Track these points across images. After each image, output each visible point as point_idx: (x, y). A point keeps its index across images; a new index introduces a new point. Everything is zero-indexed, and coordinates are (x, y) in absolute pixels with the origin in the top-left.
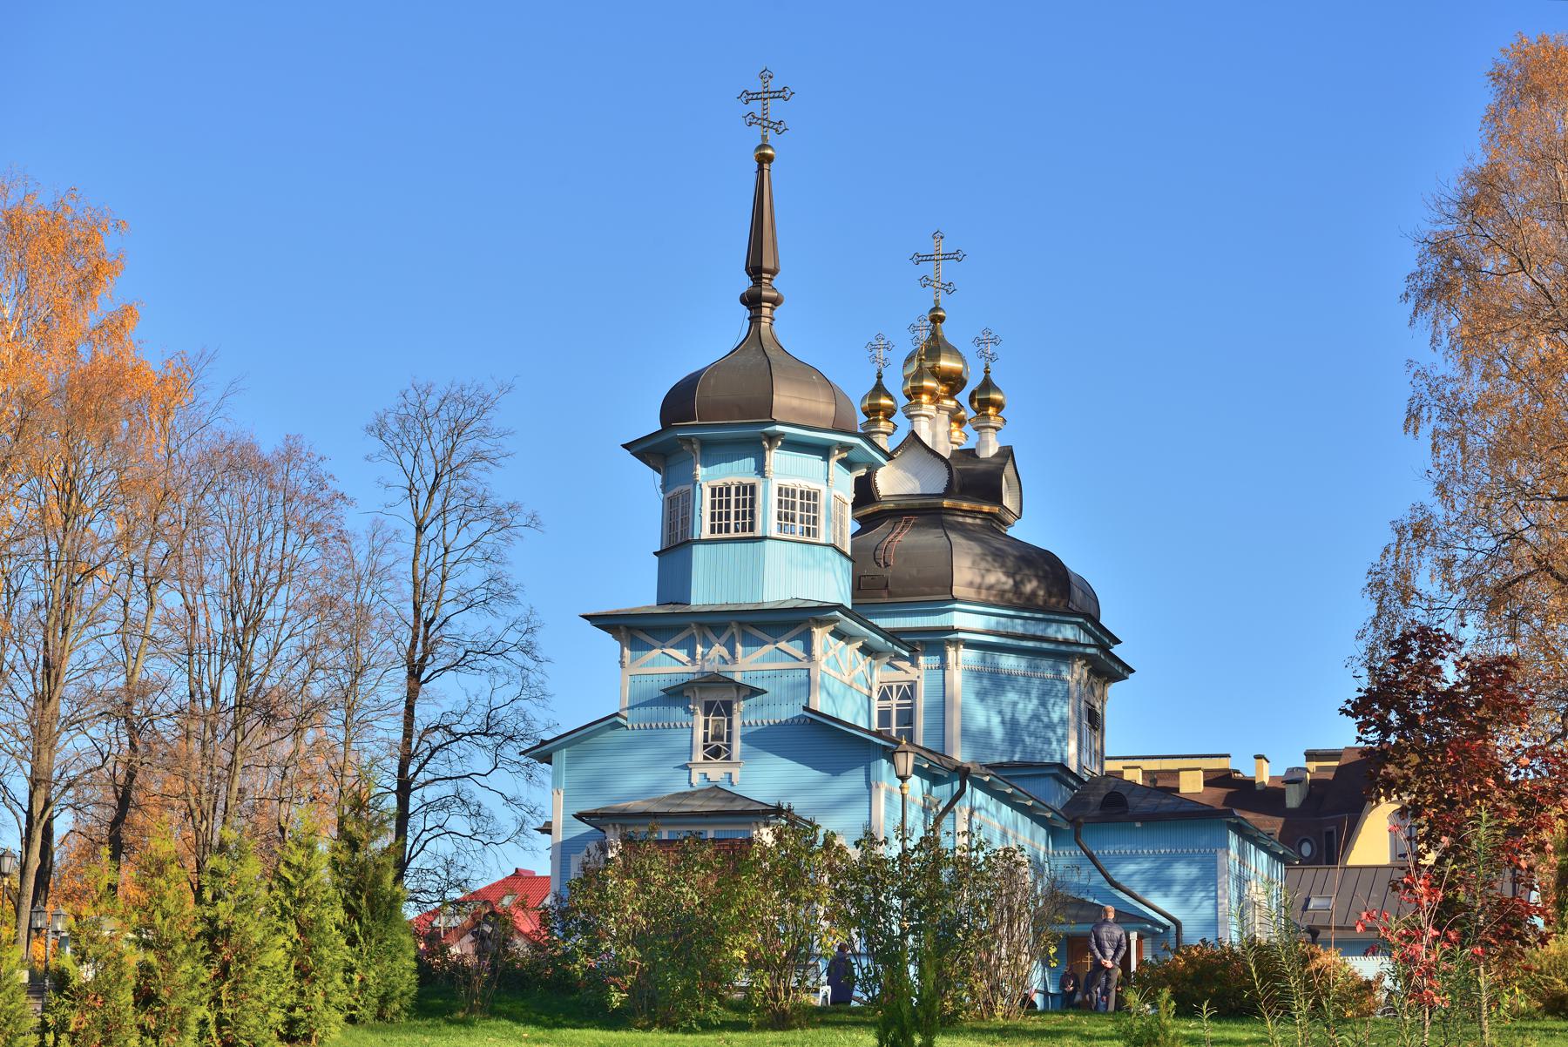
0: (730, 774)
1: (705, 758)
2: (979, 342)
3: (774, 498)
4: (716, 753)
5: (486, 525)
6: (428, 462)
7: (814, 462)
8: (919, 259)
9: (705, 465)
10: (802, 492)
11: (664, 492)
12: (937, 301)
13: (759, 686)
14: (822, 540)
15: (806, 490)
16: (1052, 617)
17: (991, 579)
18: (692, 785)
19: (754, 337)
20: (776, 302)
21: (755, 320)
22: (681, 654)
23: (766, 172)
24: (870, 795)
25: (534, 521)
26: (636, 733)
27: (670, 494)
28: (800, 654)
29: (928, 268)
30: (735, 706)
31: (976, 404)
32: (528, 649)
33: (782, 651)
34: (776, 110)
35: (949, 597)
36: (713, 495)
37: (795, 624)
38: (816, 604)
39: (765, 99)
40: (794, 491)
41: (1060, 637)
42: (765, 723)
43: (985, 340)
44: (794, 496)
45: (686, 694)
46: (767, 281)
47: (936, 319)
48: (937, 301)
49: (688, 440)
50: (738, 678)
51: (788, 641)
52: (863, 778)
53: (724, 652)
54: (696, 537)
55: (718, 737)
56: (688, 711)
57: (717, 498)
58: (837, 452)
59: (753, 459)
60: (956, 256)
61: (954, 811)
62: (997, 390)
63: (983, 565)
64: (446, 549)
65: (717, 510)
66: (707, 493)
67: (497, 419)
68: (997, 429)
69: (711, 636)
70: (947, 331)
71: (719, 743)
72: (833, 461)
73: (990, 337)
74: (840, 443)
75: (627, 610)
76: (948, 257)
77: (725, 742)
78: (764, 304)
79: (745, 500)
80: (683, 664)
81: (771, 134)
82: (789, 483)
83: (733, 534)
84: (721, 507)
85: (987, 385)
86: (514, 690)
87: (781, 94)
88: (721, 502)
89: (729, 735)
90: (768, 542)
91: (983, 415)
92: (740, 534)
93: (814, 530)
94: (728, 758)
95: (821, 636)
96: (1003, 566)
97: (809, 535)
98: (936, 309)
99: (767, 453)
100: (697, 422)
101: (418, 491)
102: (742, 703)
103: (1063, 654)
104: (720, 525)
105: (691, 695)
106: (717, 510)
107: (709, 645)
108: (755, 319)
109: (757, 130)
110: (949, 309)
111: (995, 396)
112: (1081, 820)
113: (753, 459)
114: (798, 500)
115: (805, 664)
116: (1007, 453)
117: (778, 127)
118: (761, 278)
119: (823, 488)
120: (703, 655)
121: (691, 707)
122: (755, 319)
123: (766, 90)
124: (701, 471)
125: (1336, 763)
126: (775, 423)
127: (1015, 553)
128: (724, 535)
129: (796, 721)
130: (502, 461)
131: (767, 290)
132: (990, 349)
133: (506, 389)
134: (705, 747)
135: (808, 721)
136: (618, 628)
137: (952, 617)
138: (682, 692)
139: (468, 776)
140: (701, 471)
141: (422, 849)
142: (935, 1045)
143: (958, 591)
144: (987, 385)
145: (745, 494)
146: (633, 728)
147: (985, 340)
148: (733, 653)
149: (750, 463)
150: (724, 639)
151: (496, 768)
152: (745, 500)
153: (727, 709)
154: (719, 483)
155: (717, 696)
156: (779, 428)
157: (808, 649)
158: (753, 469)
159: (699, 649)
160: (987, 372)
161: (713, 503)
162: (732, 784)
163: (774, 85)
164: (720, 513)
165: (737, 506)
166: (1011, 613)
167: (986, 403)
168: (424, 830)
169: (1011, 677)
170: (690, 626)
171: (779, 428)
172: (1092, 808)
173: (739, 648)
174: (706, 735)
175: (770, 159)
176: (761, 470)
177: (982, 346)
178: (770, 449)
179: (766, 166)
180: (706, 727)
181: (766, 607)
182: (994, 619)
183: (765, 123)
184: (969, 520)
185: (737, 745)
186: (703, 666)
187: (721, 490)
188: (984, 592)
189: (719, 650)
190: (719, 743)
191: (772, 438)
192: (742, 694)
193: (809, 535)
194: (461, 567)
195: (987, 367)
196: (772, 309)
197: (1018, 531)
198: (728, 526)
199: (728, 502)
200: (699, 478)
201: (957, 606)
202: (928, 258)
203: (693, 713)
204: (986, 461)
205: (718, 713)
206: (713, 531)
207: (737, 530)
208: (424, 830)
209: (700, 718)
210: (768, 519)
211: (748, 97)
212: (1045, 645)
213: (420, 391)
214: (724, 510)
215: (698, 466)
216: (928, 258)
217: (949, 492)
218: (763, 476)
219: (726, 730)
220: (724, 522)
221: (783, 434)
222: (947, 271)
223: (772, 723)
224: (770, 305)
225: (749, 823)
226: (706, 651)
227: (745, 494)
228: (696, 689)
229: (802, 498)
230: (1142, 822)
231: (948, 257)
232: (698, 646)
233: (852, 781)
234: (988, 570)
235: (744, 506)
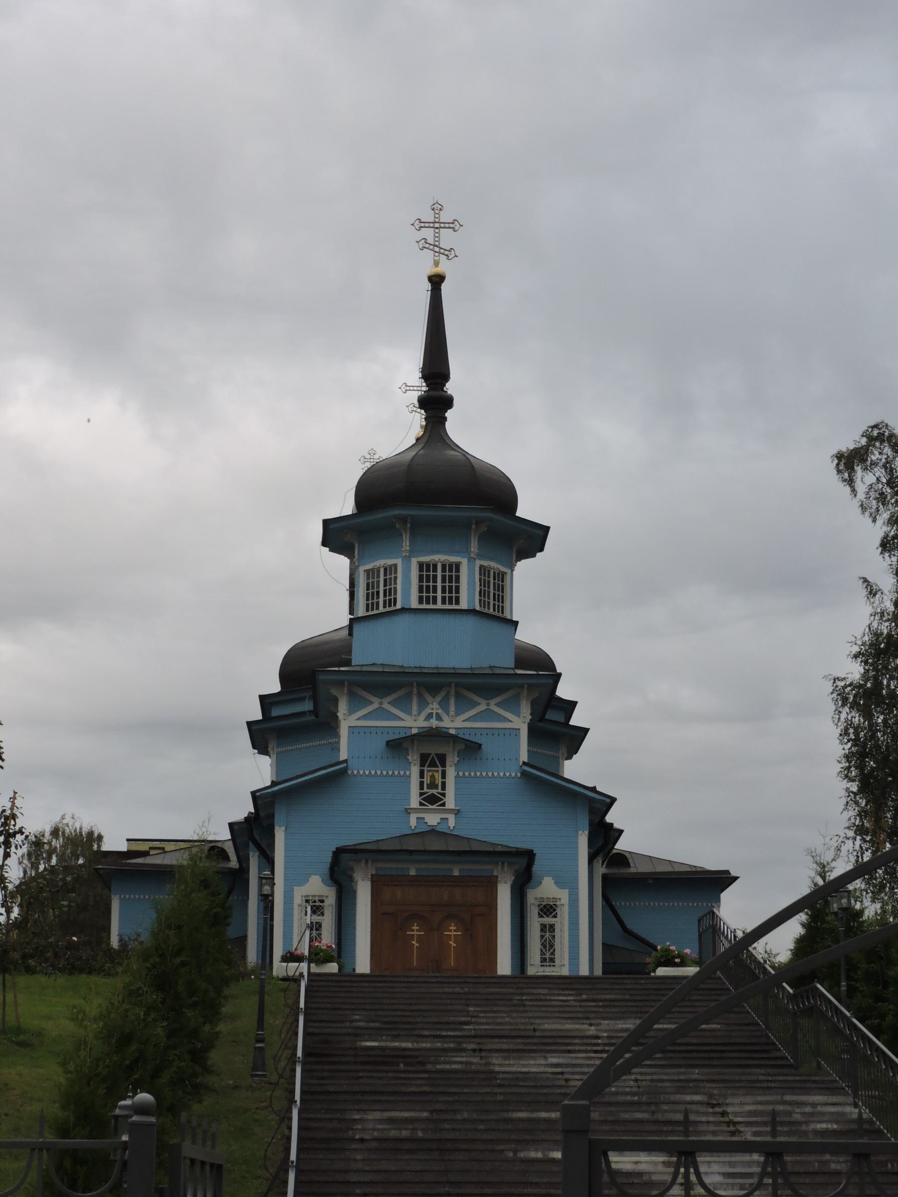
1: (421, 804)
14: (464, 605)
34: (447, 238)
36: (421, 570)
55: (433, 785)
57: (447, 573)
71: (434, 791)
77: (440, 790)
83: (439, 605)
87: (453, 225)
92: (447, 607)
114: (439, 584)
117: (448, 253)
128: (431, 606)
134: (421, 794)
142: (897, 434)
150: (439, 698)
155: (433, 750)
163: (445, 217)
170: (412, 684)
172: (889, 498)
174: (422, 784)
180: (422, 775)
183: (437, 249)
190: (434, 791)
198: (435, 599)
205: (433, 764)
206: (421, 602)
207: (444, 602)
209: (415, 771)
211: (422, 224)
214: (454, 574)
219: (440, 780)
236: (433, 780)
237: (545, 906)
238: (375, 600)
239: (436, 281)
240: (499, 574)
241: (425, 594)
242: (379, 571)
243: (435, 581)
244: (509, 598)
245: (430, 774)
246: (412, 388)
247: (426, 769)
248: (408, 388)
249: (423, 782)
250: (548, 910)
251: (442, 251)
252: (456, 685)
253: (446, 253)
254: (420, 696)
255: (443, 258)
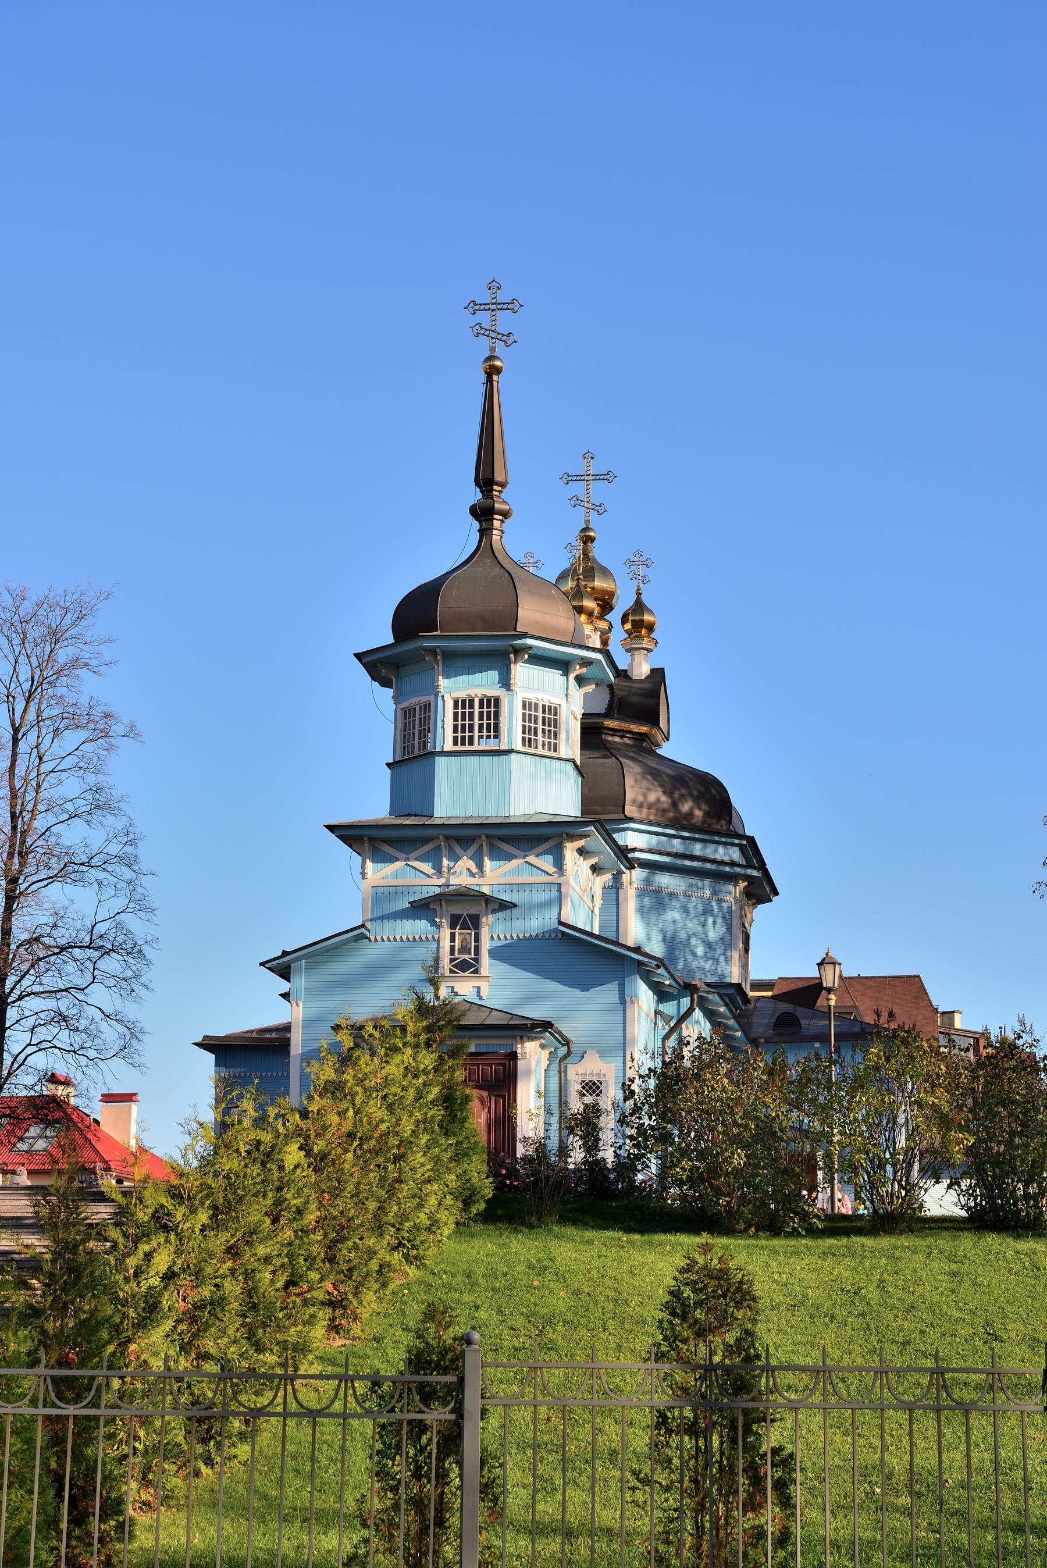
0: (479, 988)
1: (451, 971)
2: (630, 563)
3: (519, 711)
4: (464, 966)
5: (83, 735)
6: (24, 672)
7: (554, 676)
8: (570, 478)
9: (447, 676)
10: (544, 706)
11: (396, 703)
12: (587, 521)
13: (507, 897)
14: (563, 755)
15: (547, 704)
16: (697, 836)
17: (652, 797)
18: (438, 998)
19: (485, 549)
20: (506, 515)
21: (486, 532)
22: (427, 867)
23: (495, 383)
24: (624, 1011)
25: (132, 732)
26: (386, 944)
27: (405, 705)
28: (551, 869)
29: (578, 489)
30: (484, 919)
31: (628, 626)
32: (128, 861)
33: (531, 865)
34: (504, 321)
35: (622, 817)
36: (456, 706)
37: (546, 839)
38: (479, 821)
39: (493, 310)
40: (536, 705)
41: (718, 857)
42: (515, 937)
43: (638, 562)
44: (536, 710)
45: (431, 907)
46: (497, 493)
47: (588, 540)
48: (587, 521)
49: (433, 651)
50: (486, 890)
51: (537, 856)
52: (616, 994)
53: (472, 865)
54: (438, 749)
55: (464, 949)
56: (433, 923)
57: (460, 710)
58: (578, 667)
59: (496, 672)
60: (606, 477)
61: (681, 1029)
62: (650, 612)
63: (645, 784)
64: (41, 758)
65: (460, 722)
66: (450, 705)
67: (96, 626)
68: (649, 650)
69: (458, 849)
70: (599, 552)
71: (466, 957)
72: (572, 676)
73: (641, 559)
74: (582, 658)
75: (374, 820)
76: (599, 477)
77: (473, 956)
78: (495, 516)
79: (489, 713)
80: (428, 876)
81: (499, 345)
82: (532, 696)
84: (463, 719)
85: (639, 606)
86: (121, 902)
87: (509, 306)
88: (464, 714)
89: (477, 949)
90: (513, 756)
91: (636, 637)
93: (555, 744)
94: (476, 972)
95: (570, 851)
96: (662, 786)
97: (530, 746)
98: (587, 529)
99: (513, 666)
100: (438, 633)
101: (13, 697)
102: (490, 916)
103: (719, 875)
104: (463, 738)
105: (438, 908)
106: (460, 722)
107: (456, 858)
108: (485, 531)
109: (485, 343)
110: (598, 532)
111: (647, 618)
112: (762, 1040)
113: (496, 672)
115: (555, 878)
116: (658, 675)
117: (506, 338)
118: (492, 490)
119: (563, 703)
120: (449, 869)
121: (437, 920)
122: (485, 531)
123: (494, 301)
124: (443, 683)
125: (770, 994)
126: (525, 635)
127: (671, 773)
128: (467, 748)
129: (547, 935)
130: (103, 669)
131: (499, 502)
132: (642, 570)
133: (104, 596)
134: (452, 960)
135: (560, 935)
136: (363, 839)
137: (626, 837)
138: (428, 904)
139: (66, 990)
140: (443, 683)
141: (22, 1064)
143: (630, 810)
144: (639, 606)
145: (489, 706)
146: (389, 940)
147: (638, 562)
148: (480, 867)
149: (493, 675)
151: (93, 982)
152: (489, 713)
153: (474, 922)
154: (462, 694)
156: (529, 641)
157: (559, 864)
158: (496, 683)
159: (445, 862)
160: (639, 594)
161: (456, 715)
162: (481, 998)
163: (502, 297)
164: (463, 726)
165: (481, 718)
166: (672, 832)
167: (638, 625)
168: (29, 1045)
169: (673, 895)
170: (438, 838)
171: (529, 641)
173: (487, 862)
174: (452, 948)
175: (498, 371)
176: (506, 682)
177: (633, 568)
178: (515, 662)
179: (495, 378)
180: (453, 939)
181: (512, 820)
182: (655, 838)
183: (493, 335)
184: (617, 739)
185: (485, 960)
186: (448, 879)
187: (464, 701)
188: (645, 811)
189: (466, 863)
191: (518, 651)
192: (491, 907)
193: (530, 746)
194: (52, 778)
195: (639, 590)
196: (502, 521)
197: (666, 750)
199: (471, 714)
200: (441, 689)
201: (632, 825)
202: (578, 478)
203: (439, 926)
204: (641, 681)
206: (455, 743)
208: (29, 1045)
209: (446, 932)
210: (512, 733)
211: (476, 307)
212: (709, 866)
213: (14, 595)
214: (467, 722)
215: (440, 678)
216: (578, 478)
217: (608, 714)
218: (509, 689)
219: (473, 944)
220: (467, 734)
221: (530, 647)
222: (598, 491)
223: (521, 937)
224: (500, 517)
225: (515, 1037)
226: (452, 864)
227: (489, 706)
228: (444, 903)
229: (544, 712)
230: (821, 1042)
231: (599, 477)
232: (445, 859)
233: (606, 994)
234: (649, 789)
235: (489, 718)
236: (464, 944)
237: (587, 1084)
238: (411, 742)
239: (492, 372)
240: (550, 707)
241: (460, 735)
242: (414, 709)
243: (481, 714)
244: (398, 731)
245: (462, 937)
246: (602, 477)
247: (457, 931)
248: (606, 477)
249: (454, 946)
250: (590, 1088)
251: (499, 337)
252: (488, 837)
253: (504, 338)
254: (450, 849)
255: (500, 344)
